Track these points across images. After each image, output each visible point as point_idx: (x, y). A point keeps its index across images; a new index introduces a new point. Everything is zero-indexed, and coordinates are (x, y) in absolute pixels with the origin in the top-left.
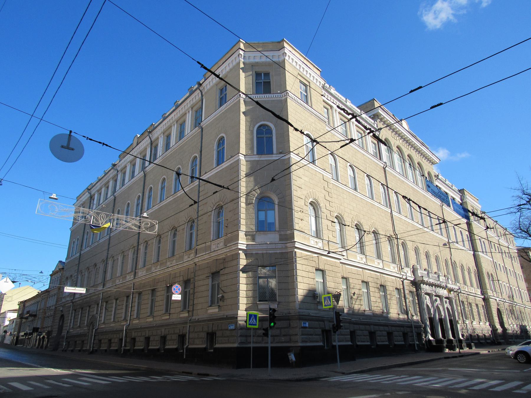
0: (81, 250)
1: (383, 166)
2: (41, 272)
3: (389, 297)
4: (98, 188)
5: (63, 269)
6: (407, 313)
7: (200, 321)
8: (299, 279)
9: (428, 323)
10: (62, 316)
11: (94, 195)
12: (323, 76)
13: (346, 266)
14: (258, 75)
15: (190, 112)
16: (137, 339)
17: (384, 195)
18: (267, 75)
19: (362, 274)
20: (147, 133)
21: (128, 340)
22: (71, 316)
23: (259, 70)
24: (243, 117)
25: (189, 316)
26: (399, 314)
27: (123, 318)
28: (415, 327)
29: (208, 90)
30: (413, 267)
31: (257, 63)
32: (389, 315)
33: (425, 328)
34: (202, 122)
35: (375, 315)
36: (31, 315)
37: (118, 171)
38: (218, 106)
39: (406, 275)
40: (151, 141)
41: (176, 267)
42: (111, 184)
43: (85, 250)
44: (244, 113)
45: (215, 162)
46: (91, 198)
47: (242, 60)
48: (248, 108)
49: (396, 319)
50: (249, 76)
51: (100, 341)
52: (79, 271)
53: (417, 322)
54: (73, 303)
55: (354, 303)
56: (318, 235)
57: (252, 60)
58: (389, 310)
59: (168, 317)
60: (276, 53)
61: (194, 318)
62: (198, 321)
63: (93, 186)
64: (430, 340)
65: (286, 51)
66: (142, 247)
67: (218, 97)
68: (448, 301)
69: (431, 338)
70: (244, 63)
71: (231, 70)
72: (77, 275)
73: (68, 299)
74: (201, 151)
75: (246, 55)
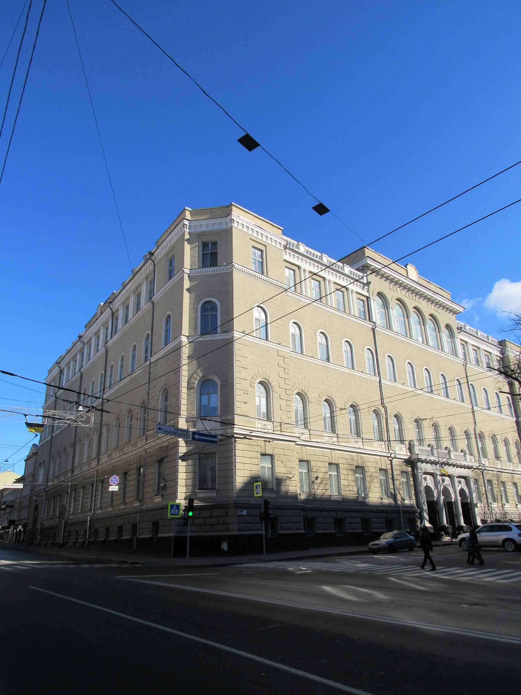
0: (53, 432)
1: (371, 326)
2: (7, 461)
3: (368, 479)
4: (66, 362)
5: (36, 453)
6: (394, 497)
7: (150, 511)
8: (238, 466)
9: (425, 507)
10: (37, 506)
11: (64, 369)
12: (284, 233)
13: (307, 447)
14: (205, 245)
15: (145, 283)
16: (100, 530)
17: (371, 361)
18: (215, 244)
19: (329, 455)
20: (108, 304)
21: (92, 531)
22: (45, 507)
23: (205, 239)
24: (186, 296)
25: (140, 506)
26: (382, 498)
27: (89, 508)
28: (403, 513)
29: (160, 261)
30: (409, 444)
31: (204, 232)
32: (367, 500)
33: (421, 514)
34: (154, 295)
35: (345, 501)
36: (8, 506)
37: (84, 344)
38: (167, 279)
39: (395, 453)
40: (113, 312)
41: (130, 454)
42: (78, 357)
43: (54, 435)
44: (188, 290)
45: (163, 341)
46: (61, 372)
47: (187, 230)
48: (193, 283)
49: (379, 504)
50: (195, 247)
51: (69, 532)
52: (50, 456)
53: (412, 506)
54: (46, 491)
55: (316, 487)
56: (268, 417)
57: (198, 230)
58: (368, 494)
59: (124, 507)
60: (224, 220)
61: (143, 507)
62: (147, 511)
63: (62, 358)
64: (425, 528)
65: (233, 218)
66: (104, 431)
67: (167, 270)
68: (463, 480)
69: (428, 524)
70: (190, 234)
71: (178, 240)
72: (49, 460)
73: (42, 487)
74: (152, 329)
75: (191, 225)
